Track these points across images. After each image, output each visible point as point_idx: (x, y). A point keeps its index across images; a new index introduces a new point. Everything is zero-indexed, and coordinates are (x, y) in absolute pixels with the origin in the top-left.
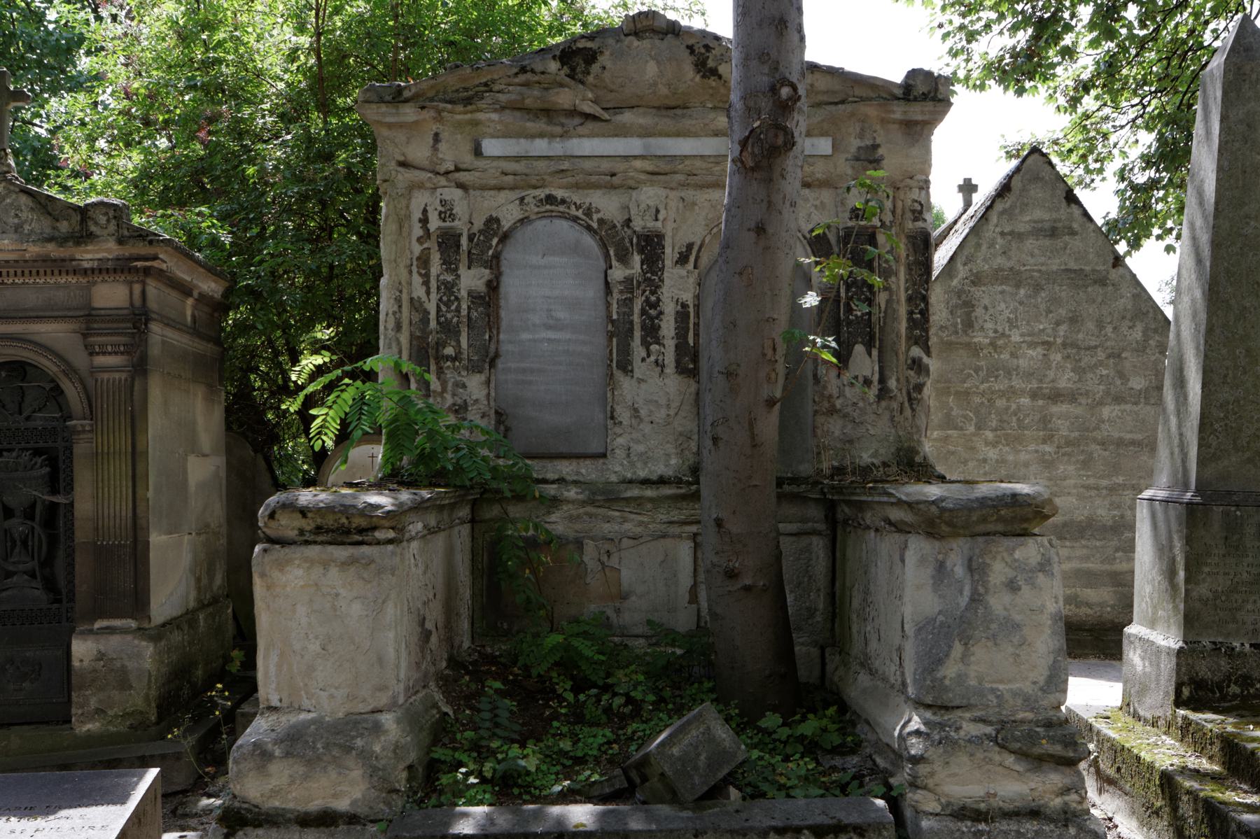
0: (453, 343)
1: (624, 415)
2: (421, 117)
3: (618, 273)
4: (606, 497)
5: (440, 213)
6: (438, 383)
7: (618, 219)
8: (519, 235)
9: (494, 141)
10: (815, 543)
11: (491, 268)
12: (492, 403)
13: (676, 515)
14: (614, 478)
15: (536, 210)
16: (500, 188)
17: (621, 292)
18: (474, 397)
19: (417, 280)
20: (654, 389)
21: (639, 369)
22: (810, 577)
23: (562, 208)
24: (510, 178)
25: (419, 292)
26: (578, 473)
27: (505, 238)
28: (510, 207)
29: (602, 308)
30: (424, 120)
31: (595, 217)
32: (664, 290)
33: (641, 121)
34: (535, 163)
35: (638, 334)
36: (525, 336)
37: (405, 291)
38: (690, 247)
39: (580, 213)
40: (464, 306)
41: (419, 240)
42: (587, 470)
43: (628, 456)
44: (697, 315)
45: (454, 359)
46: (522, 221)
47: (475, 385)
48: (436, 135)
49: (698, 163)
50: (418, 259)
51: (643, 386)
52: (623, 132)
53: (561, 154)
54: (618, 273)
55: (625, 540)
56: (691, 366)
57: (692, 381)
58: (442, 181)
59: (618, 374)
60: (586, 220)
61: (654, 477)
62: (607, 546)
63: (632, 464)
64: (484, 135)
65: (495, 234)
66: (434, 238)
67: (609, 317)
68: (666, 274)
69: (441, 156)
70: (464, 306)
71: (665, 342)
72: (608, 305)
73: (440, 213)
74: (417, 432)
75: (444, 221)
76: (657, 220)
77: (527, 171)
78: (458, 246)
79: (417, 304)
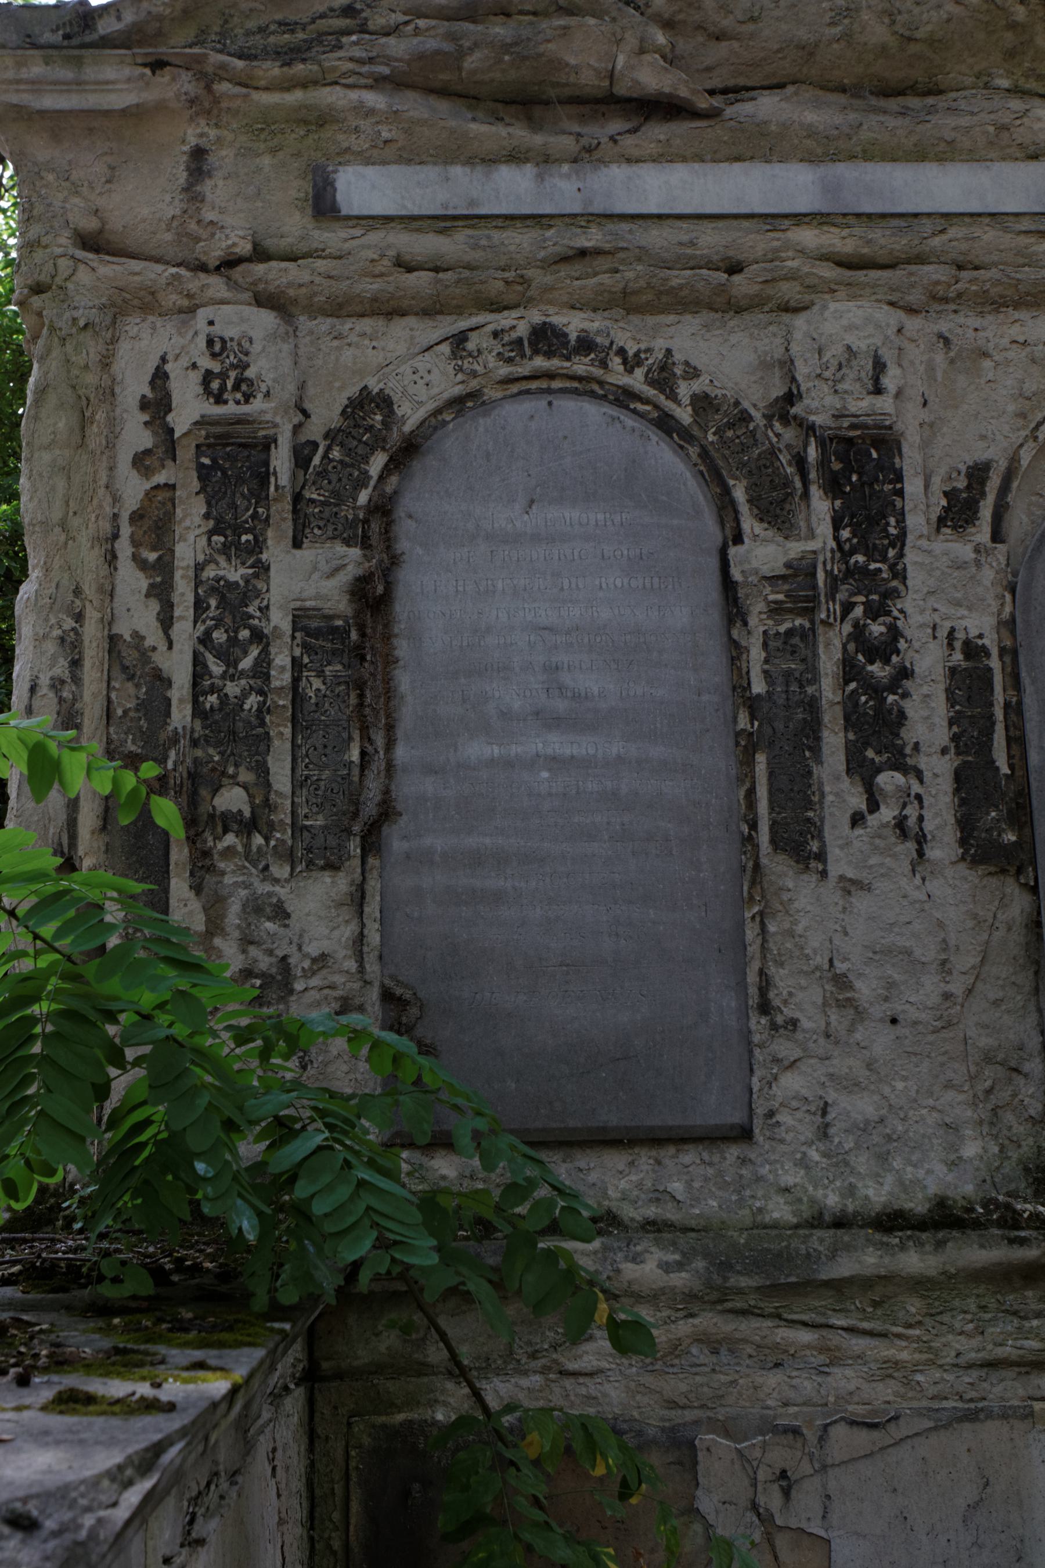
0: (246, 776)
1: (802, 998)
2: (149, 96)
3: (763, 553)
4: (769, 1276)
5: (208, 377)
6: (195, 905)
7: (756, 395)
8: (450, 443)
9: (371, 172)
11: (365, 544)
12: (372, 968)
13: (1006, 1339)
14: (780, 1211)
15: (504, 370)
16: (390, 310)
17: (776, 610)
18: (313, 949)
19: (132, 581)
20: (889, 906)
21: (845, 849)
23: (581, 366)
24: (421, 280)
25: (139, 617)
26: (660, 1196)
27: (407, 452)
28: (423, 363)
29: (715, 658)
30: (160, 107)
31: (685, 390)
33: (811, 117)
34: (497, 236)
35: (834, 741)
36: (477, 750)
37: (92, 616)
38: (978, 473)
39: (637, 380)
40: (281, 659)
41: (141, 461)
42: (690, 1184)
43: (824, 1132)
44: (1015, 680)
45: (248, 826)
46: (458, 404)
47: (316, 911)
48: (198, 154)
49: (989, 235)
50: (136, 517)
51: (861, 903)
52: (760, 146)
53: (577, 209)
54: (763, 553)
55: (840, 1432)
56: (1011, 837)
57: (1011, 887)
58: (216, 286)
59: (779, 868)
60: (655, 399)
61: (918, 1205)
62: (779, 1456)
63: (840, 1161)
64: (346, 155)
65: (378, 443)
66: (186, 453)
67: (740, 687)
68: (911, 557)
69: (209, 215)
70: (281, 659)
71: (923, 762)
72: (736, 652)
73: (208, 377)
74: (117, 1058)
75: (219, 400)
76: (878, 390)
77: (477, 256)
78: (263, 476)
79: (130, 657)
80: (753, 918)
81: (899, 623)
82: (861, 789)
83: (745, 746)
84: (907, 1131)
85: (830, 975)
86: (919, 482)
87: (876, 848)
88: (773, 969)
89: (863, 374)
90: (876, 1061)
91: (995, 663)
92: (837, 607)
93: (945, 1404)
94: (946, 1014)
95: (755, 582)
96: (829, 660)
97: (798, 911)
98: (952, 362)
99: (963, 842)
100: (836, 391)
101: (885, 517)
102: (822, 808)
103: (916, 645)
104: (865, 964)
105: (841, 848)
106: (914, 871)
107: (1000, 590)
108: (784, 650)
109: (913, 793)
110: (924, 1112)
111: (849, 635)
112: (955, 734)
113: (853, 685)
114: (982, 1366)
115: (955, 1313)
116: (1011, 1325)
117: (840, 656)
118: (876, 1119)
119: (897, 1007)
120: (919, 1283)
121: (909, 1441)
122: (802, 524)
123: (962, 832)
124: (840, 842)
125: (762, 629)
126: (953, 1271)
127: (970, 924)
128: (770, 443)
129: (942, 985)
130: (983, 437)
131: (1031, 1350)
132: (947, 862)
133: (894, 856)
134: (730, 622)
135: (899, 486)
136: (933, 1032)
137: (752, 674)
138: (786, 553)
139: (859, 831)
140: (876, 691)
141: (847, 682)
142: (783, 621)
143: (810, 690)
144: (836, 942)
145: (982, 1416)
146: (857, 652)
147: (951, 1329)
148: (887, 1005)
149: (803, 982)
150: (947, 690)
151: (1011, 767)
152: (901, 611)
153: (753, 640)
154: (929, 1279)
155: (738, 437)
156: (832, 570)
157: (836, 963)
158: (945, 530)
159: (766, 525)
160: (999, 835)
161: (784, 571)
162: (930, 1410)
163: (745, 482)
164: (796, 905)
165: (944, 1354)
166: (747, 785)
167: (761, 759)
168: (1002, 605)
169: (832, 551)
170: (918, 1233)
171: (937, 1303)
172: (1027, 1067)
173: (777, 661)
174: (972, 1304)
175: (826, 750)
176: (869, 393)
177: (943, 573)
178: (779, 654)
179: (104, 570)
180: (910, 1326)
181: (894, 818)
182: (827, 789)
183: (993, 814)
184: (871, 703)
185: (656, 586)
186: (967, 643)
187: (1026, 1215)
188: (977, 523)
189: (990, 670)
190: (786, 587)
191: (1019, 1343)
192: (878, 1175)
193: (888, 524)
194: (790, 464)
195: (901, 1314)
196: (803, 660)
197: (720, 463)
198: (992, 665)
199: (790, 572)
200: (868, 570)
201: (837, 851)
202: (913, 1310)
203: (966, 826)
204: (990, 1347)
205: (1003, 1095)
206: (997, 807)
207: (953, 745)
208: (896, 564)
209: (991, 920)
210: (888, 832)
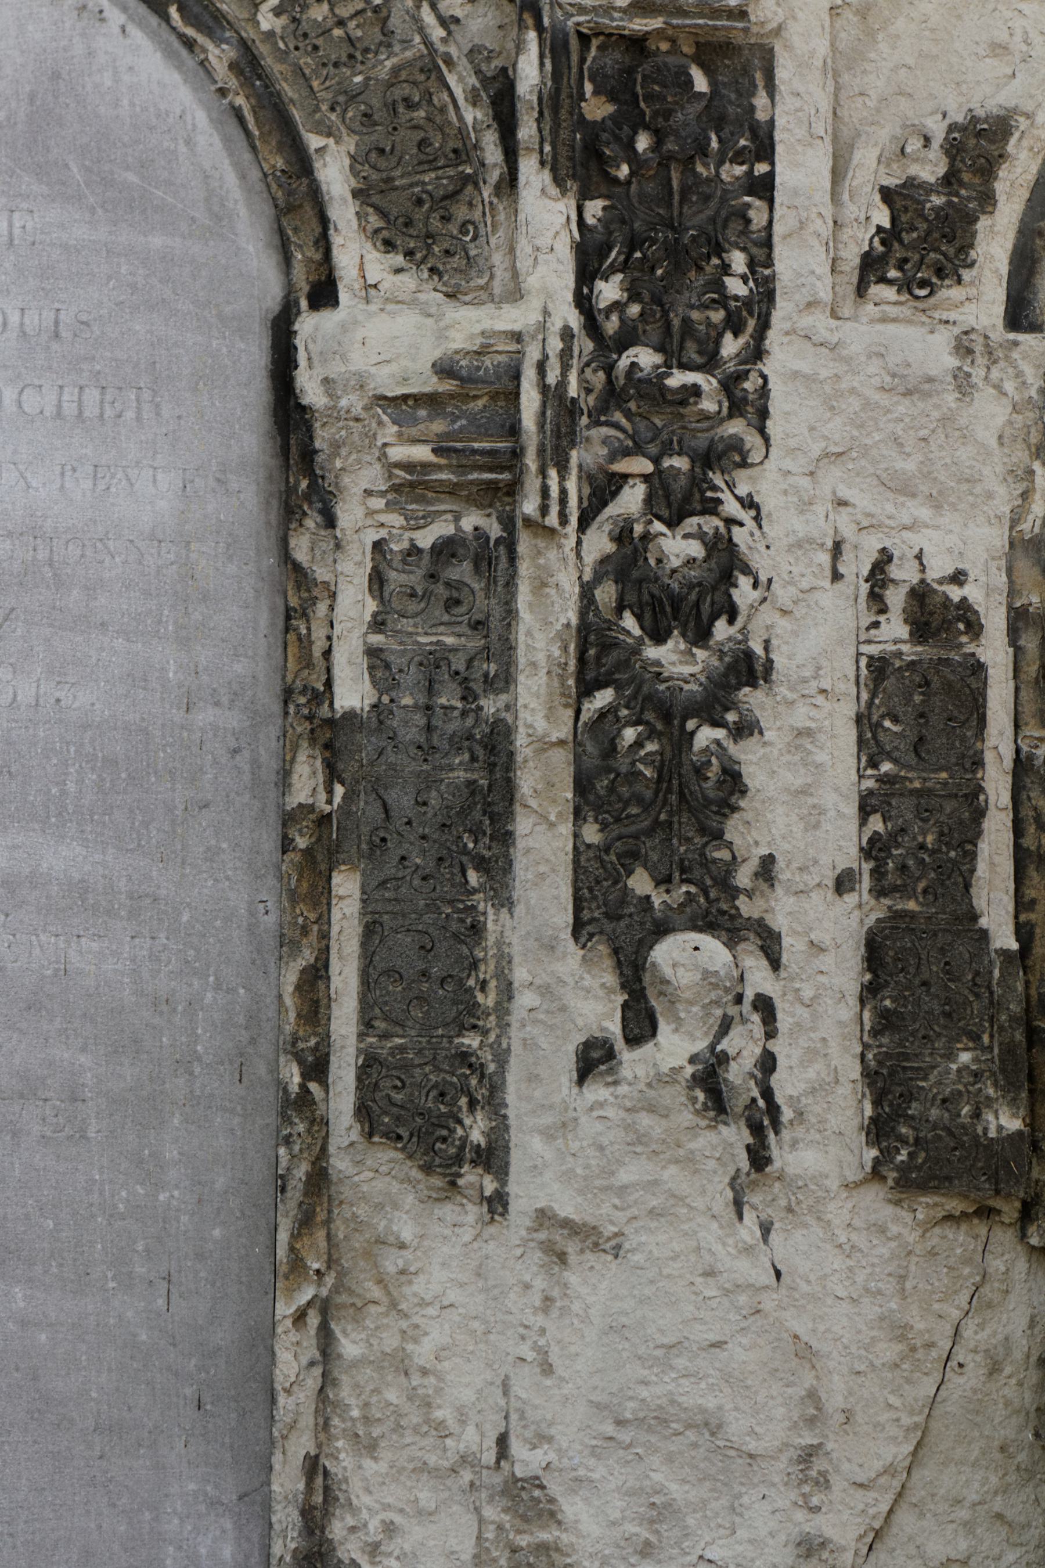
3: (385, 333)
17: (410, 487)
21: (559, 1135)
32: (768, 480)
35: (545, 844)
38: (977, 147)
51: (592, 1283)
54: (385, 333)
59: (375, 1180)
67: (303, 696)
68: (782, 358)
71: (781, 910)
72: (298, 596)
80: (300, 1317)
81: (739, 535)
82: (610, 979)
83: (308, 852)
85: (497, 1479)
86: (820, 160)
87: (641, 1139)
88: (347, 1460)
91: (994, 651)
92: (572, 485)
95: (358, 410)
96: (543, 625)
97: (423, 1304)
99: (878, 1130)
101: (719, 250)
102: (504, 1026)
104: (594, 1452)
105: (548, 1134)
106: (738, 1205)
108: (427, 595)
109: (749, 995)
111: (604, 560)
113: (604, 698)
122: (497, 259)
123: (876, 1103)
124: (548, 1119)
125: (372, 536)
127: (888, 1351)
128: (427, 42)
129: (800, 1515)
130: (998, 49)
132: (833, 1184)
133: (689, 1162)
134: (289, 512)
135: (761, 168)
137: (339, 658)
138: (441, 336)
139: (596, 1091)
140: (667, 717)
141: (586, 689)
142: (429, 518)
143: (490, 705)
144: (518, 1389)
146: (620, 609)
149: (426, 1497)
150: (859, 719)
152: (748, 503)
153: (346, 566)
155: (341, 23)
156: (563, 384)
157: (517, 1448)
158: (878, 291)
159: (399, 260)
160: (977, 1115)
161: (432, 384)
163: (350, 143)
164: (419, 1286)
166: (307, 957)
167: (347, 886)
169: (567, 334)
173: (406, 625)
175: (523, 870)
177: (867, 405)
178: (413, 607)
181: (693, 1060)
182: (520, 974)
183: (965, 1057)
184: (651, 747)
185: (91, 411)
186: (920, 595)
188: (966, 275)
189: (978, 668)
190: (438, 426)
193: (726, 269)
194: (474, 100)
196: (477, 625)
197: (288, 90)
198: (985, 655)
199: (448, 386)
200: (663, 389)
201: (537, 1144)
203: (890, 1090)
206: (976, 1038)
207: (867, 866)
208: (741, 376)
210: (675, 1096)
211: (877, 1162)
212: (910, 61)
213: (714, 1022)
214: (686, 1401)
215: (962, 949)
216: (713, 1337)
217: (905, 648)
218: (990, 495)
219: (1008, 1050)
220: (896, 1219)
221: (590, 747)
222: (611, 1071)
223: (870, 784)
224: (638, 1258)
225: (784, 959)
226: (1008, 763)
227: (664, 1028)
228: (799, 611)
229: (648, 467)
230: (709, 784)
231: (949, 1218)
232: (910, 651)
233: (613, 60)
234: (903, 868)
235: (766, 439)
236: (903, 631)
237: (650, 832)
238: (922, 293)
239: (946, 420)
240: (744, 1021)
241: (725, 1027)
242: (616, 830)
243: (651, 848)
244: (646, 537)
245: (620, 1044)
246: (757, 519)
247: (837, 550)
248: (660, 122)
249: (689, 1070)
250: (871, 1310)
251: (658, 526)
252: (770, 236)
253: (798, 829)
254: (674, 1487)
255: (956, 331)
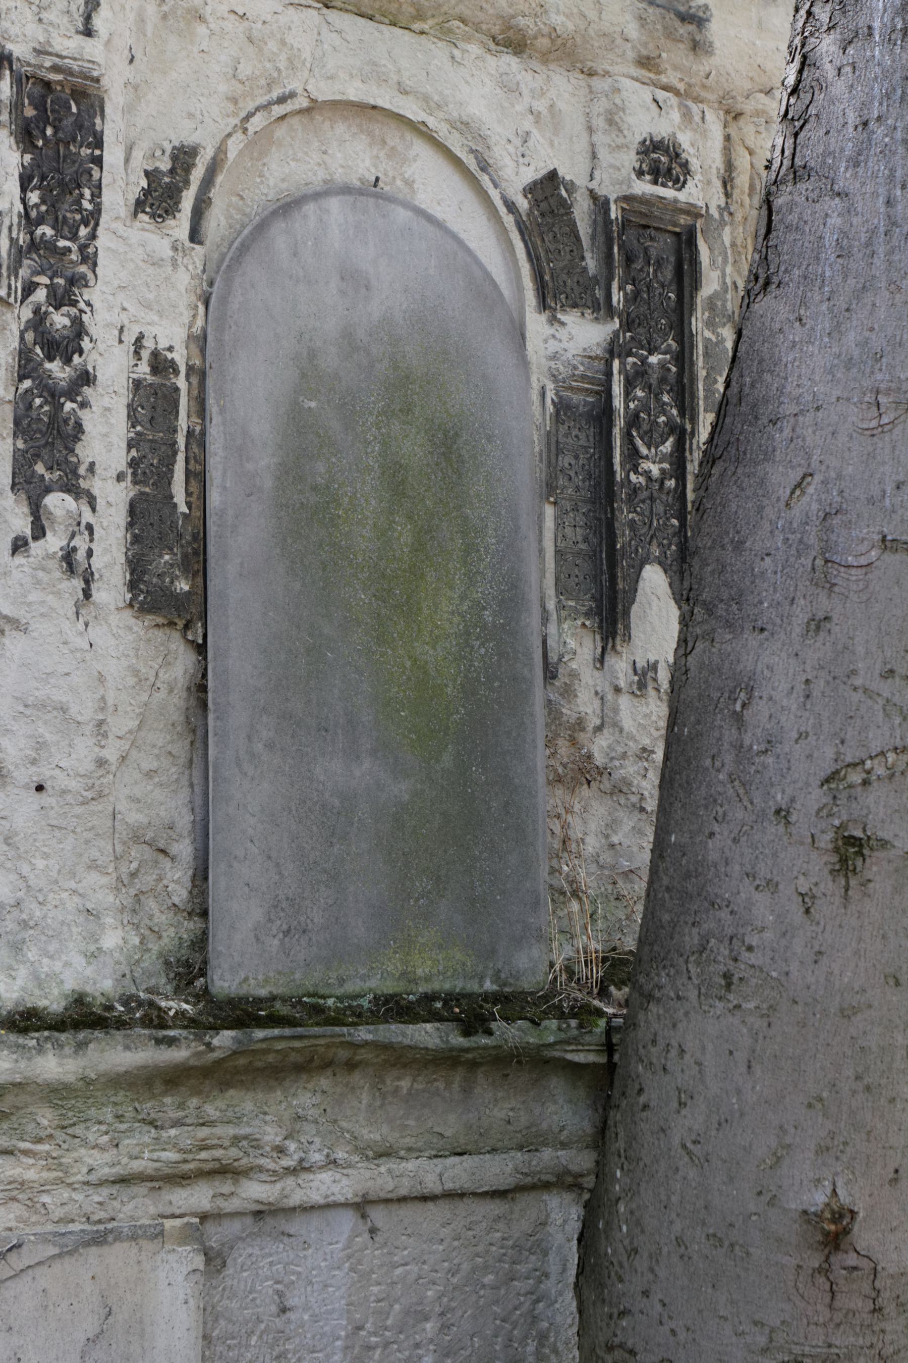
10: (557, 1217)
13: (144, 1151)
22: (542, 1337)
38: (184, 157)
56: (183, 586)
61: (53, 1002)
68: (103, 241)
76: (88, 32)
81: (85, 318)
82: (26, 510)
84: (45, 917)
87: (39, 582)
89: (73, 8)
90: (17, 834)
91: (181, 382)
93: (71, 1227)
94: (98, 783)
98: (165, 17)
99: (132, 586)
100: (40, 20)
101: (79, 187)
103: (101, 346)
104: (14, 718)
106: (77, 613)
107: (193, 298)
110: (65, 895)
111: (28, 322)
112: (133, 459)
113: (27, 383)
114: (114, 1182)
115: (89, 1124)
116: (148, 1135)
117: (16, 344)
118: (12, 902)
119: (44, 773)
120: (55, 1091)
121: (30, 1271)
123: (132, 574)
126: (93, 1076)
127: (131, 681)
129: (97, 749)
130: (191, 116)
131: (168, 1163)
132: (112, 607)
133: (58, 594)
135: (97, 152)
136: (83, 804)
139: (19, 559)
140: (53, 395)
141: (21, 378)
145: (110, 1238)
146: (35, 344)
147: (85, 1143)
148: (34, 769)
150: (128, 406)
151: (189, 505)
152: (88, 304)
154: (67, 1087)
156: (18, 239)
158: (142, 216)
160: (172, 582)
162: (56, 1234)
165: (75, 1170)
168: (194, 316)
170: (56, 1034)
171: (70, 1114)
172: (175, 849)
174: (108, 1114)
176: (78, 32)
179: (411, 98)
180: (39, 1140)
181: (61, 549)
183: (167, 557)
184: (46, 408)
187: (171, 1013)
188: (177, 214)
189: (177, 390)
191: (155, 1155)
192: (10, 968)
193: (82, 196)
195: (31, 1127)
200: (56, 246)
202: (45, 1122)
203: (137, 570)
204: (125, 1160)
205: (147, 880)
206: (171, 549)
207: (130, 471)
209: (152, 679)
210: (53, 564)
211: (131, 599)
212: (154, 114)
213: (69, 533)
214: (54, 698)
215: (166, 511)
216: (66, 671)
217: (148, 377)
218: (181, 314)
219: (185, 556)
220: (136, 625)
221: (21, 406)
222: (26, 551)
223: (132, 435)
224: (35, 634)
225: (98, 508)
226: (185, 433)
227: (49, 534)
228: (106, 355)
229: (48, 282)
230: (69, 428)
231: (157, 625)
232: (150, 379)
233: (38, 90)
234: (145, 473)
235: (96, 276)
236: (147, 369)
237: (45, 446)
238: (160, 220)
239: (167, 279)
240: (81, 533)
241: (73, 536)
242: (31, 444)
243: (45, 453)
244: (46, 313)
245: (30, 540)
246: (92, 311)
247: (121, 330)
248: (57, 123)
249: (60, 553)
250: (124, 663)
251: (51, 309)
252: (100, 184)
253: (104, 451)
254: (47, 735)
255: (173, 239)
